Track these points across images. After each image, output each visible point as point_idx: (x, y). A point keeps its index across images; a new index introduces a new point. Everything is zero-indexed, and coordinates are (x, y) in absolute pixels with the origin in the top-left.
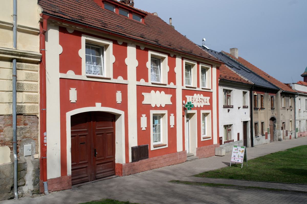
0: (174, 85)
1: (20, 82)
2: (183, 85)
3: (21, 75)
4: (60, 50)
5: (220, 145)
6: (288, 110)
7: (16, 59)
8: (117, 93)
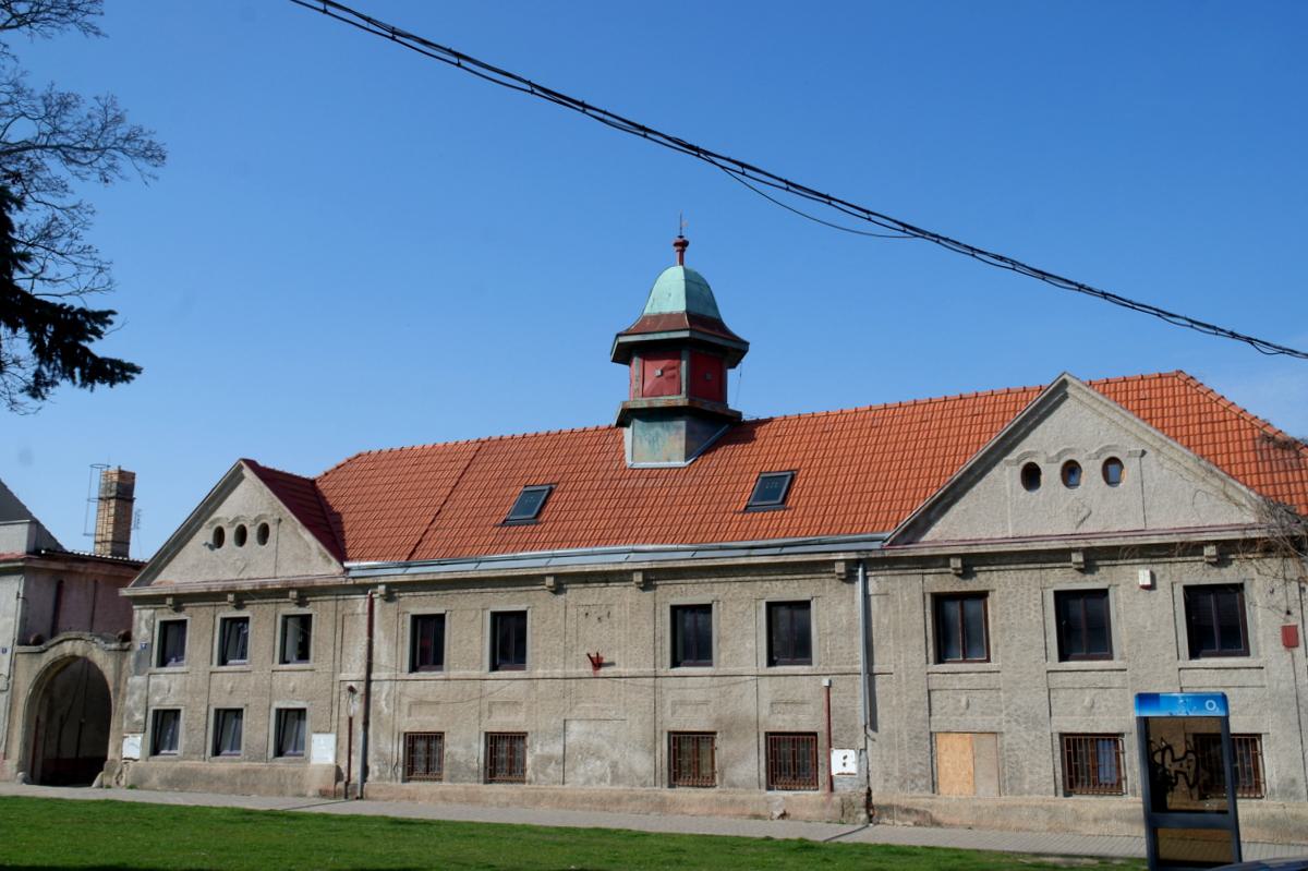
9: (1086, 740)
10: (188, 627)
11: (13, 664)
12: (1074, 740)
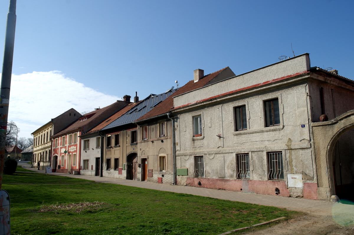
9: (276, 154)
10: (247, 109)
11: (312, 133)
12: (245, 156)
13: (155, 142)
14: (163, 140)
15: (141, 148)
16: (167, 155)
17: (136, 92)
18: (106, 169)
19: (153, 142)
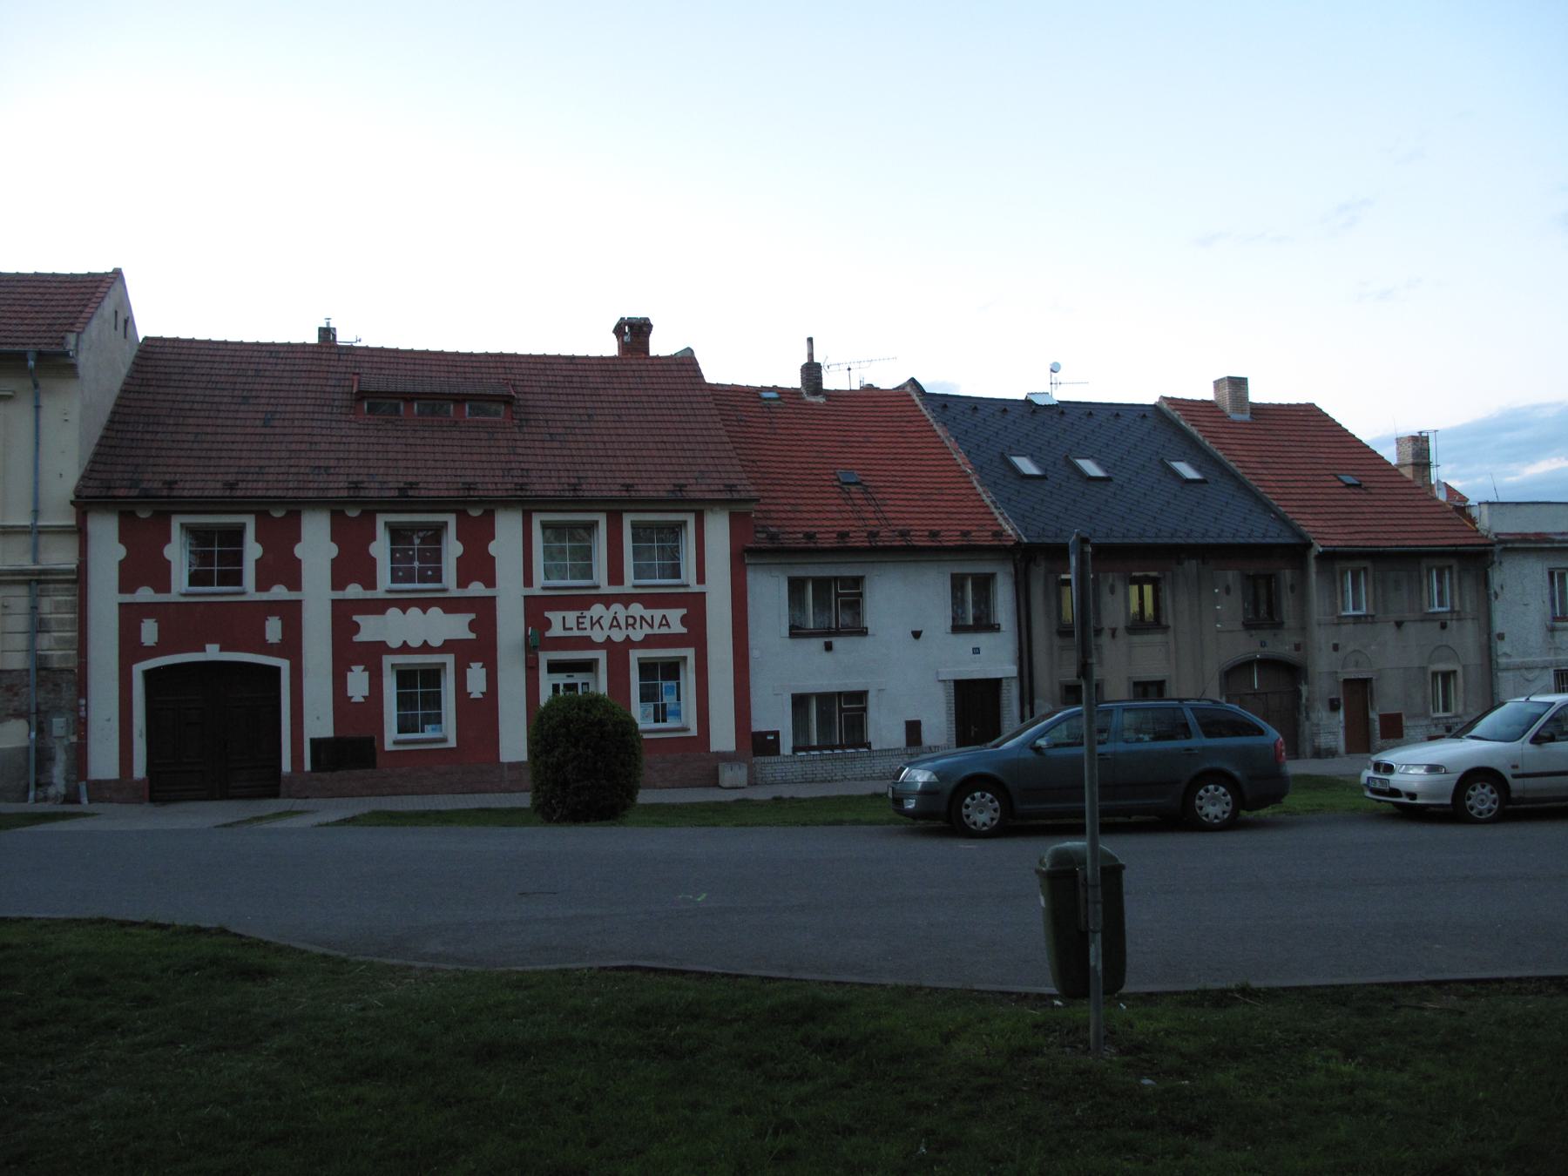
0: (484, 588)
1: (44, 616)
2: (528, 581)
3: (46, 605)
4: (121, 552)
5: (776, 752)
6: (1399, 624)
7: (36, 580)
8: (267, 623)
13: (1411, 629)
14: (1446, 623)
15: (1335, 642)
16: (1464, 667)
17: (810, 340)
18: (79, 806)
19: (1399, 624)
